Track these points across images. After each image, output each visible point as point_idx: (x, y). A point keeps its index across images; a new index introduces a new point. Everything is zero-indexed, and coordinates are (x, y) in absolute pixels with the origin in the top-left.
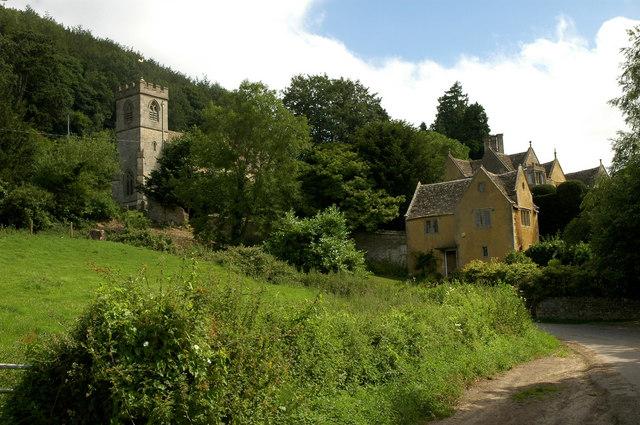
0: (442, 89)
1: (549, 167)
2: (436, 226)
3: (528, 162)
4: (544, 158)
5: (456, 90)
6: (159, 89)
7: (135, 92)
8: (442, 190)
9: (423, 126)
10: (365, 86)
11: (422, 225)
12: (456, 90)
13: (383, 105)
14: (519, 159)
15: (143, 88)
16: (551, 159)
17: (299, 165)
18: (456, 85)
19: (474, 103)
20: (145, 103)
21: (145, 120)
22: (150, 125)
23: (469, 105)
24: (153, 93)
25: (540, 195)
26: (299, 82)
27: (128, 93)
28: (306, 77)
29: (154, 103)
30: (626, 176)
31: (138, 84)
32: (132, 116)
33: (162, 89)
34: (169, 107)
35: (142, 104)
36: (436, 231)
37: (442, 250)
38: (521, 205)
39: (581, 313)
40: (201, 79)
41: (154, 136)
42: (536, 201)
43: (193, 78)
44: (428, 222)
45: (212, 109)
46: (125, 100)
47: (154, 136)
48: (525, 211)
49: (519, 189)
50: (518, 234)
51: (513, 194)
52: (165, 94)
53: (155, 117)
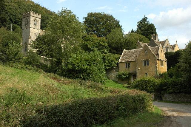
0: (140, 18)
1: (174, 46)
3: (166, 44)
4: (172, 43)
5: (144, 19)
6: (37, 14)
7: (29, 15)
11: (124, 65)
12: (144, 19)
14: (163, 43)
15: (31, 14)
16: (174, 43)
17: (81, 41)
20: (32, 19)
21: (32, 25)
24: (36, 16)
25: (167, 55)
26: (91, 15)
27: (26, 16)
28: (93, 13)
29: (35, 19)
30: (146, 26)
31: (30, 13)
32: (28, 24)
33: (39, 15)
35: (31, 20)
38: (160, 58)
39: (179, 99)
41: (35, 30)
42: (166, 57)
44: (126, 64)
46: (25, 18)
47: (35, 30)
48: (162, 61)
49: (160, 52)
50: (159, 69)
51: (158, 54)
52: (40, 16)
53: (35, 24)
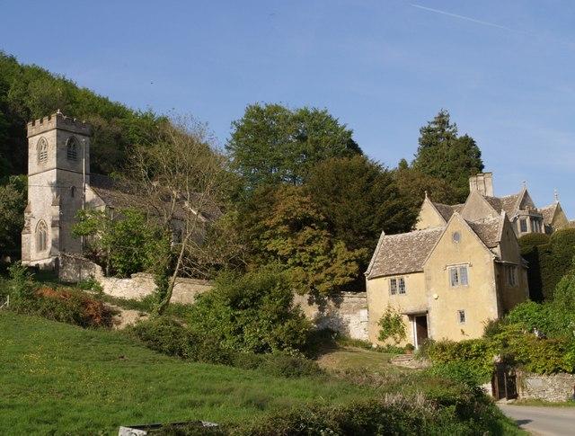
0: (427, 118)
2: (402, 285)
5: (442, 121)
8: (410, 241)
9: (403, 164)
10: (335, 118)
11: (385, 282)
12: (442, 121)
13: (354, 137)
18: (442, 116)
19: (463, 135)
22: (41, 170)
23: (458, 137)
28: (263, 107)
34: (529, 279)
35: (54, 160)
36: (403, 292)
37: (412, 316)
40: (144, 110)
43: (135, 109)
45: (60, 142)
46: (38, 137)
